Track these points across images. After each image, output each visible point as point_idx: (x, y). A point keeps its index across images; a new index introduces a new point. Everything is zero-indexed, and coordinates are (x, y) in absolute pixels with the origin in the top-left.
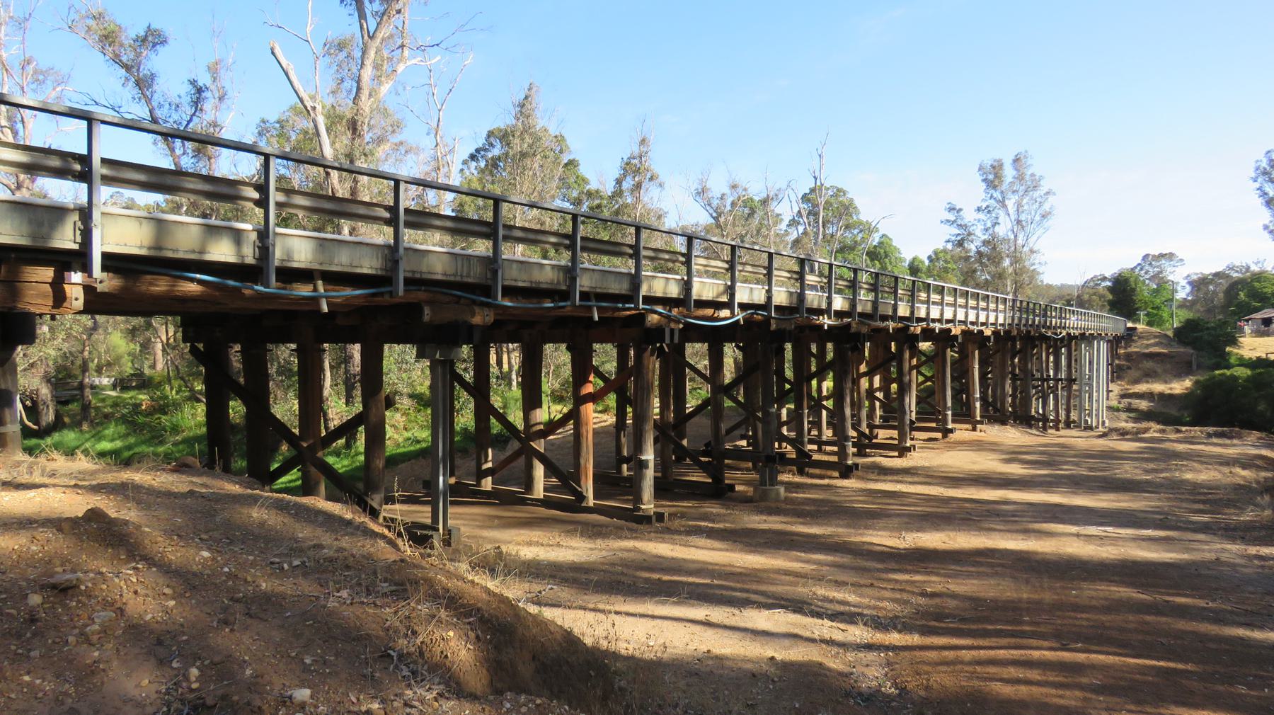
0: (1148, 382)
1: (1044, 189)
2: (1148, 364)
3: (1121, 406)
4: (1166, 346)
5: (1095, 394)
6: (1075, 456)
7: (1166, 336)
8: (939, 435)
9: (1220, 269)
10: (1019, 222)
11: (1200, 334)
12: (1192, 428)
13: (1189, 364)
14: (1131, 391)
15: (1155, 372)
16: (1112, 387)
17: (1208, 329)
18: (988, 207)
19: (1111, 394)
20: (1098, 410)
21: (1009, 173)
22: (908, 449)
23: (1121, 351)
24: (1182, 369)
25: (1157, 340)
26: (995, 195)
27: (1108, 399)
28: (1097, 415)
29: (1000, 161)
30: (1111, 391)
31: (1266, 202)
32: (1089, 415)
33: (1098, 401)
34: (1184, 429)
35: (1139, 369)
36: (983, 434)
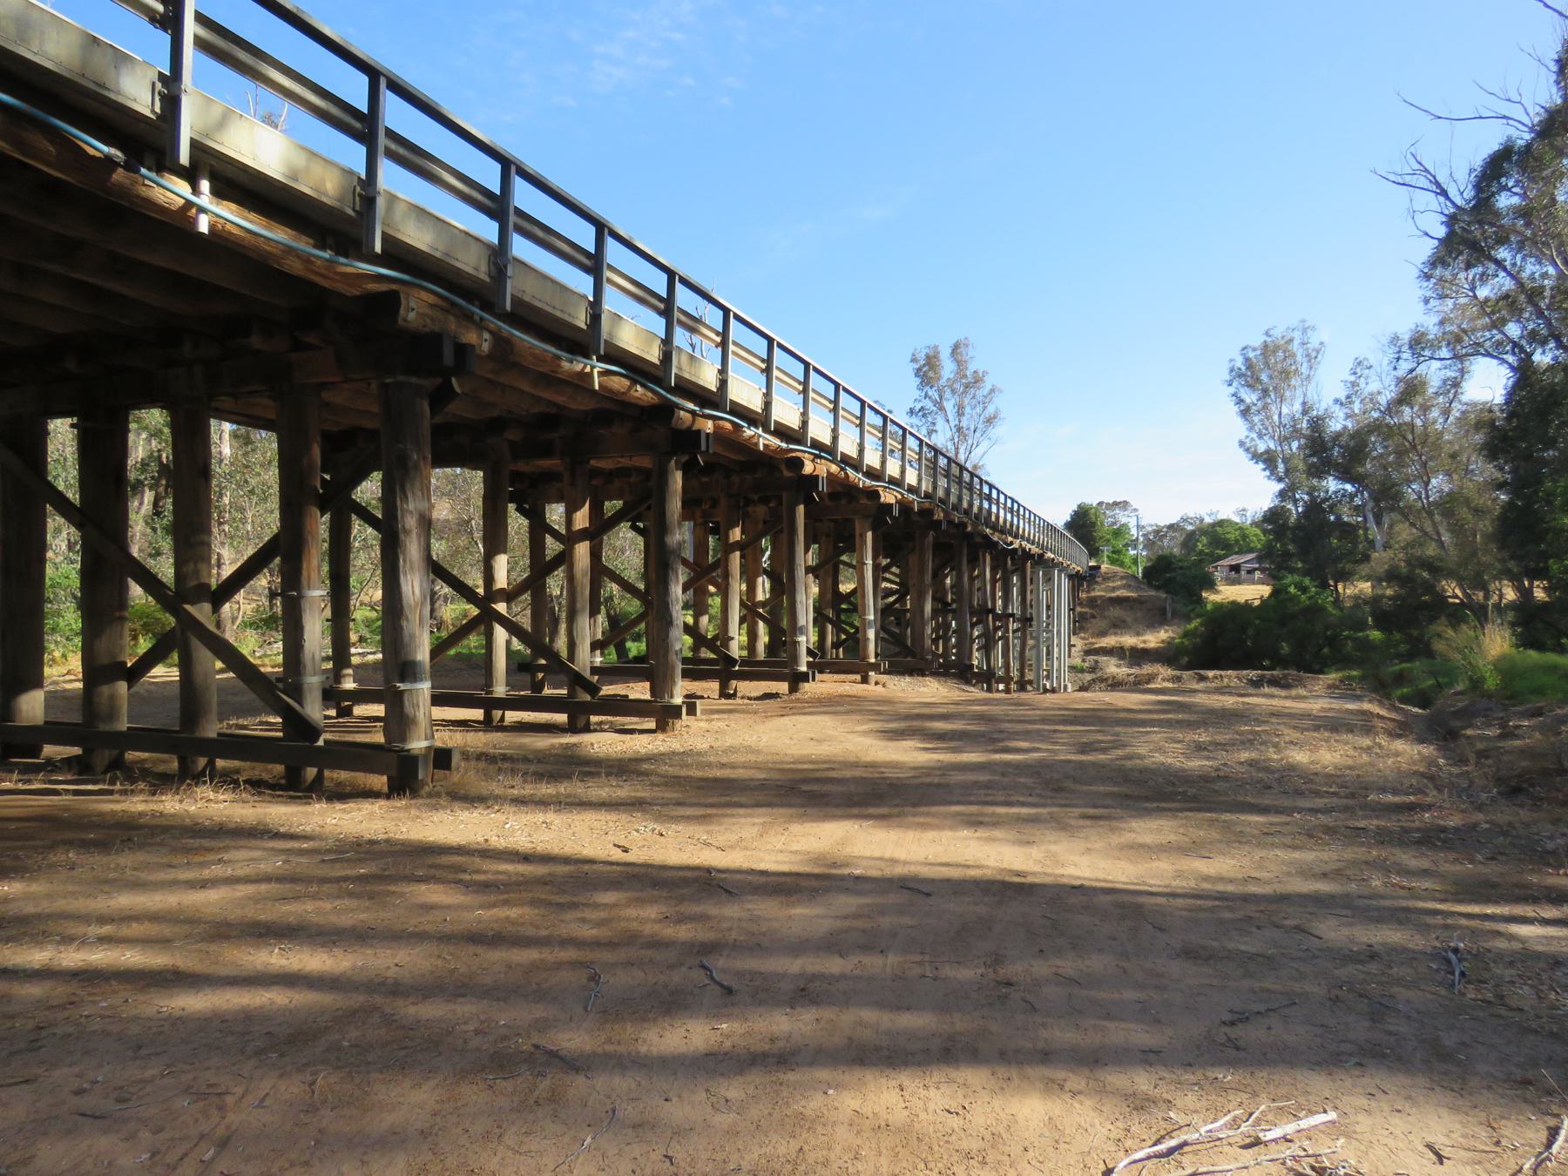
0: (1116, 634)
1: (988, 386)
2: (1115, 612)
3: (1087, 665)
4: (1137, 588)
5: (1056, 650)
6: (1044, 720)
7: (1134, 577)
8: (783, 687)
9: (1174, 521)
10: (959, 429)
11: (1173, 574)
12: (1223, 673)
13: (1163, 611)
14: (1097, 646)
15: (1124, 621)
16: (1074, 640)
17: (1181, 568)
18: (922, 409)
19: (1073, 649)
20: (1059, 671)
21: (948, 369)
22: (675, 712)
23: (1083, 595)
24: (1158, 618)
25: (1124, 582)
26: (930, 393)
27: (1069, 656)
28: (1058, 678)
29: (936, 347)
30: (1074, 646)
31: (1241, 411)
32: (1048, 677)
33: (1059, 659)
34: (1211, 674)
35: (1105, 617)
36: (879, 688)
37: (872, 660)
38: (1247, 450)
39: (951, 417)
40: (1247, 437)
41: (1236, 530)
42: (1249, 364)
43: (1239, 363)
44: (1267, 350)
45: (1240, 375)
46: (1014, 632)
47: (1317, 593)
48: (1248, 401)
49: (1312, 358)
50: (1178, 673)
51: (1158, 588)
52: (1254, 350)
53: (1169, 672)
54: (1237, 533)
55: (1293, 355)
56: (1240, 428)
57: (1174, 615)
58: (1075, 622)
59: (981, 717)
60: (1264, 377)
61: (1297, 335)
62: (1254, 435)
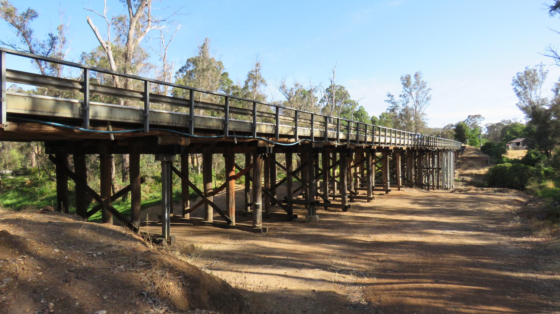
0: (470, 169)
2: (470, 162)
3: (460, 179)
4: (478, 154)
5: (449, 174)
7: (478, 150)
8: (384, 192)
9: (499, 122)
10: (417, 101)
11: (491, 149)
12: (488, 188)
13: (487, 162)
14: (464, 173)
15: (473, 165)
16: (456, 171)
18: (404, 95)
19: (455, 174)
20: (450, 181)
21: (413, 80)
24: (484, 164)
26: (407, 90)
27: (454, 176)
28: (450, 183)
29: (409, 75)
30: (456, 173)
33: (450, 177)
34: (485, 189)
35: (467, 164)
36: (403, 192)
37: (401, 185)
38: (519, 106)
39: (414, 97)
40: (519, 102)
41: (520, 128)
42: (520, 78)
43: (516, 78)
44: (527, 73)
45: (517, 82)
46: (435, 172)
47: (541, 156)
48: (519, 91)
49: (544, 75)
50: (477, 188)
51: (486, 153)
52: (522, 73)
53: (475, 188)
54: (521, 130)
55: (537, 75)
56: (517, 100)
57: (491, 163)
58: (456, 165)
59: (428, 200)
60: (525, 83)
61: (538, 69)
62: (522, 102)
